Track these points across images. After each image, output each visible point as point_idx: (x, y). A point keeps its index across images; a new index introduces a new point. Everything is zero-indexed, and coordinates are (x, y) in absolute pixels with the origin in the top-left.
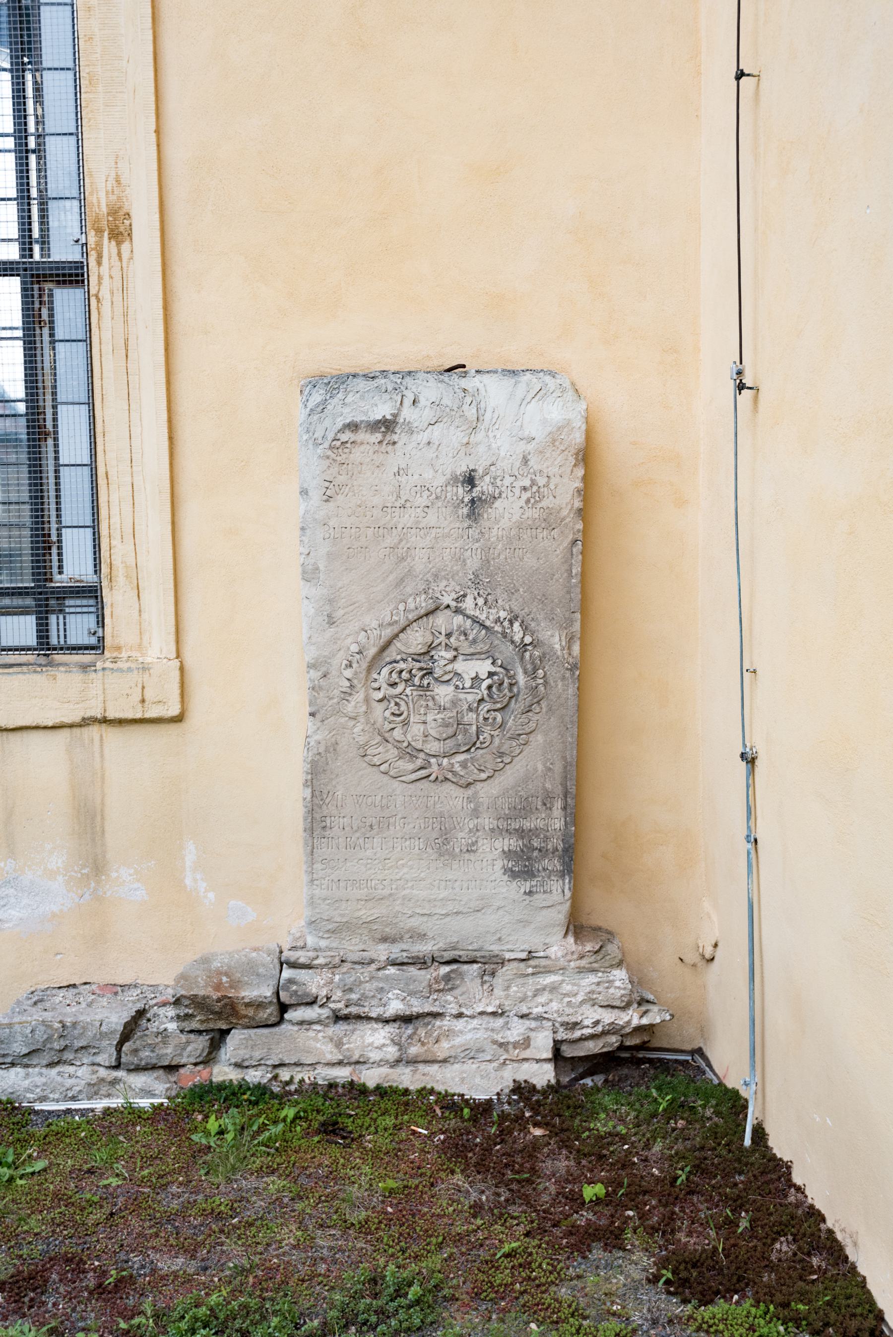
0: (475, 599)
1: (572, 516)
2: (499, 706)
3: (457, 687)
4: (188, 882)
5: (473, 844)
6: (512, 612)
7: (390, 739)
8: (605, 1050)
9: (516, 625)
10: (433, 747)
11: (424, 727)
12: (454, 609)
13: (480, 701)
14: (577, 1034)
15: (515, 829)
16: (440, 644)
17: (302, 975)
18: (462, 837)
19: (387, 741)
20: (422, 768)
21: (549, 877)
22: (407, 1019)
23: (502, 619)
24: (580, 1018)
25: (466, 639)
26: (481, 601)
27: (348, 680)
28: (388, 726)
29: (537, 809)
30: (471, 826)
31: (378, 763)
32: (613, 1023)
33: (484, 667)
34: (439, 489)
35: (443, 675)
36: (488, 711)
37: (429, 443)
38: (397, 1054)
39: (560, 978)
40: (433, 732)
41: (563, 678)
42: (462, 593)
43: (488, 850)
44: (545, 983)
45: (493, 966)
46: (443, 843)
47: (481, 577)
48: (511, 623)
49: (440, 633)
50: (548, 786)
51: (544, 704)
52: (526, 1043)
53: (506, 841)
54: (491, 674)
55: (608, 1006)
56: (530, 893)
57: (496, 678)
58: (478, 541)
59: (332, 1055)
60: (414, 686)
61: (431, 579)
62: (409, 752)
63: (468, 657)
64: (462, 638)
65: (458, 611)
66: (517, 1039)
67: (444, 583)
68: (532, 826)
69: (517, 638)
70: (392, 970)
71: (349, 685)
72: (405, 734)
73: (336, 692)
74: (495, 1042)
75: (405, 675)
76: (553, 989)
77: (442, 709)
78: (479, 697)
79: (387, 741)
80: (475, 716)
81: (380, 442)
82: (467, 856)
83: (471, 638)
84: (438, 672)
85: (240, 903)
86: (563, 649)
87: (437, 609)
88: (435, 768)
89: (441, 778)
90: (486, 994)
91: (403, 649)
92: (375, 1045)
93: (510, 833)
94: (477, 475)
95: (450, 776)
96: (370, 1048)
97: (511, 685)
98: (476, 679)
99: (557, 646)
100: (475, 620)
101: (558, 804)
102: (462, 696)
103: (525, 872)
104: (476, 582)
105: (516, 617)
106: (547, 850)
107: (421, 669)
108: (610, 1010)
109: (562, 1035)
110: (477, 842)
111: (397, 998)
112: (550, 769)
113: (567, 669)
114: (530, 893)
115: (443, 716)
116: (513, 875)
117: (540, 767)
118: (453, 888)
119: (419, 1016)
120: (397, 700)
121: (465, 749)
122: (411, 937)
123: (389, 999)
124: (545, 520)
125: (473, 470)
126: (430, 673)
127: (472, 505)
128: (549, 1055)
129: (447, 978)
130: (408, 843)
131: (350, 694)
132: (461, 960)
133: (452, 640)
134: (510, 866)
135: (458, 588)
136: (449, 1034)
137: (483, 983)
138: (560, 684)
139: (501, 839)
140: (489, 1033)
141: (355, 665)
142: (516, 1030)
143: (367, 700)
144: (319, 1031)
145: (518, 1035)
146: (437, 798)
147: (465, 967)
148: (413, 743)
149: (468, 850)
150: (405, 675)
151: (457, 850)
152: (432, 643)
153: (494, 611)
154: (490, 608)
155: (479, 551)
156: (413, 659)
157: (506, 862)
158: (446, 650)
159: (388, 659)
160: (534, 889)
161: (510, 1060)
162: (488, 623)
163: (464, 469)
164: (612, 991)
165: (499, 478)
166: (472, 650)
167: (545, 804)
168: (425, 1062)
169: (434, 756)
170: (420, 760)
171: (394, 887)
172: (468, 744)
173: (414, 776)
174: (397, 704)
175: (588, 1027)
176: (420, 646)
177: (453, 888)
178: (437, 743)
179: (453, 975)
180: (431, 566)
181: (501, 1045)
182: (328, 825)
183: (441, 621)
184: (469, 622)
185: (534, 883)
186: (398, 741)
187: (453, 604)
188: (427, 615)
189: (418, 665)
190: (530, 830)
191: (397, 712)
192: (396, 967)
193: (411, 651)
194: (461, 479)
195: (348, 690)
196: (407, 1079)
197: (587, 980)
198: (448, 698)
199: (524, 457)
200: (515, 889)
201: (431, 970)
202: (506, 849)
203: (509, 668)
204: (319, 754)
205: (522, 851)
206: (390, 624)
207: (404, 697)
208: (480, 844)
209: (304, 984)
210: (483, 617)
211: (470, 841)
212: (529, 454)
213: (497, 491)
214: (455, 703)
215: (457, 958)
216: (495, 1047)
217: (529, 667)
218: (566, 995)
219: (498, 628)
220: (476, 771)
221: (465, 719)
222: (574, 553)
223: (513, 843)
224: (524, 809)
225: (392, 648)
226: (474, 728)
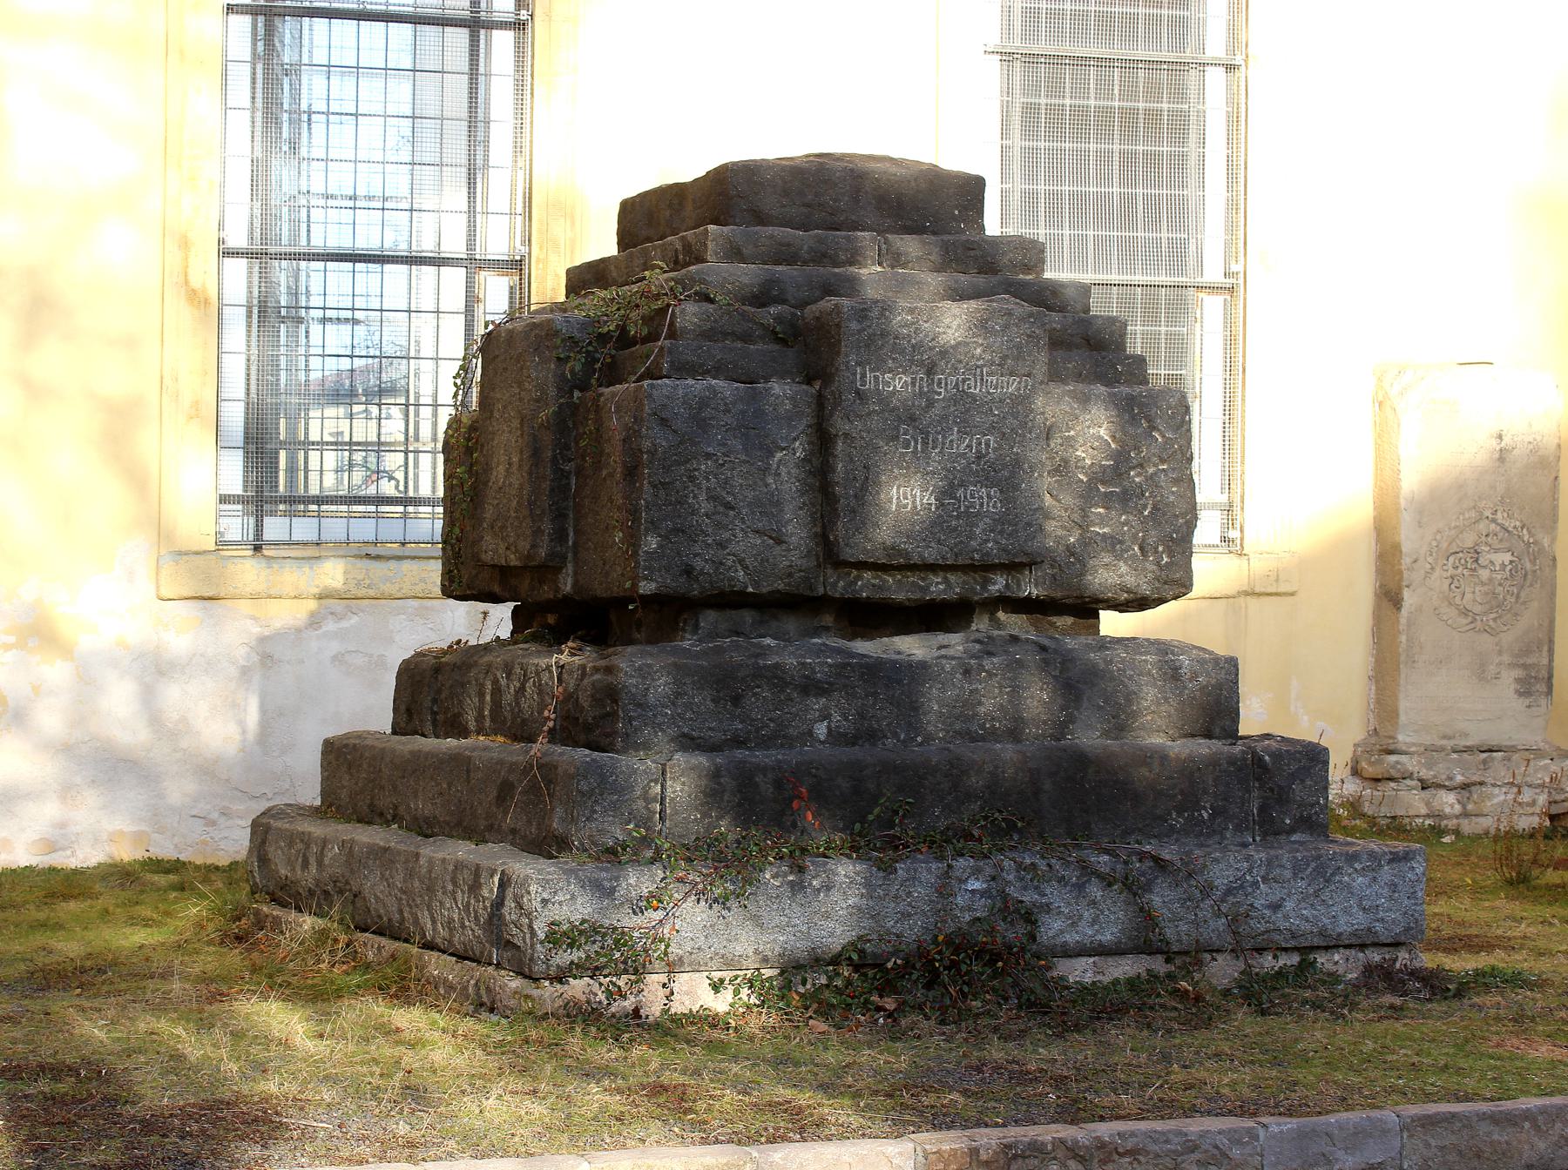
4: (1292, 708)
10: (1478, 609)
11: (1472, 596)
17: (1403, 758)
18: (1492, 668)
22: (1465, 786)
33: (1507, 557)
46: (1481, 673)
59: (1424, 811)
62: (1465, 612)
65: (1494, 521)
70: (1455, 756)
77: (1483, 584)
98: (1503, 565)
101: (1546, 648)
104: (1502, 502)
116: (1520, 694)
119: (1474, 784)
129: (1484, 762)
183: (1482, 526)
200: (1519, 704)
214: (1491, 580)
223: (1519, 673)
224: (1527, 652)
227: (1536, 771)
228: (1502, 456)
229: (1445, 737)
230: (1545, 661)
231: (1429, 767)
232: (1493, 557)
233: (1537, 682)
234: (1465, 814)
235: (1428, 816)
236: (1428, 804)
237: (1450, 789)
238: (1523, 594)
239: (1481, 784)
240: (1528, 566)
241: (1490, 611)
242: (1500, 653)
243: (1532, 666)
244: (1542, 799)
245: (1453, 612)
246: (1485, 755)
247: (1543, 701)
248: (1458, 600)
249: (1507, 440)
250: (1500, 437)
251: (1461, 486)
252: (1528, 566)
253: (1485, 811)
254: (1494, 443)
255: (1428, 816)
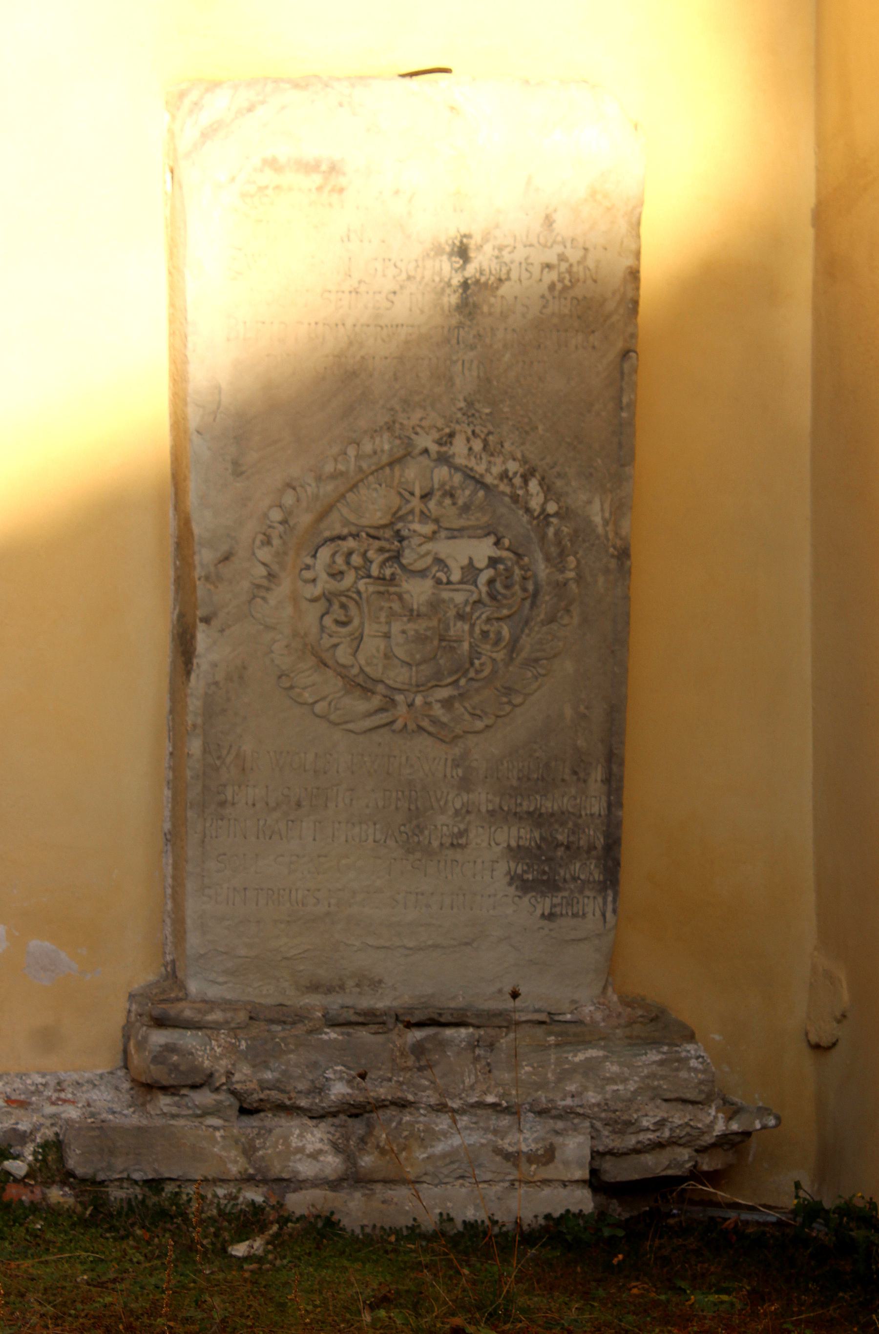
0: (468, 440)
1: (621, 311)
2: (505, 612)
3: (439, 582)
5: (461, 834)
6: (526, 462)
7: (330, 662)
8: (670, 1172)
9: (534, 485)
10: (399, 676)
11: (381, 644)
12: (434, 455)
13: (475, 602)
14: (631, 1141)
15: (529, 813)
16: (412, 512)
17: (189, 1040)
18: (444, 823)
19: (325, 665)
20: (382, 710)
21: (581, 892)
22: (356, 1110)
23: (510, 474)
24: (635, 1116)
25: (454, 504)
26: (477, 445)
27: (264, 564)
28: (327, 642)
29: (563, 780)
30: (458, 806)
31: (311, 700)
32: (687, 1124)
33: (482, 550)
34: (413, 264)
35: (415, 561)
36: (488, 620)
37: (397, 192)
38: (341, 1167)
39: (601, 1053)
40: (399, 652)
41: (607, 571)
42: (447, 430)
43: (485, 844)
44: (577, 1059)
45: (491, 1032)
46: (413, 831)
47: (477, 406)
48: (525, 480)
49: (412, 494)
50: (580, 743)
51: (576, 610)
52: (549, 1155)
53: (514, 831)
54: (493, 562)
55: (677, 1100)
56: (550, 917)
57: (501, 567)
58: (472, 347)
60: (369, 576)
61: (398, 407)
62: (361, 685)
63: (456, 533)
64: (448, 501)
65: (444, 459)
66: (533, 1146)
67: (419, 414)
68: (556, 807)
69: (535, 503)
70: (332, 1035)
71: (265, 573)
72: (355, 654)
73: (245, 585)
74: (498, 1151)
75: (356, 560)
76: (590, 1068)
77: (413, 615)
78: (475, 597)
79: (325, 665)
80: (467, 627)
81: (319, 189)
82: (450, 853)
83: (460, 502)
84: (408, 558)
85: (47, 944)
86: (606, 523)
87: (408, 454)
88: (402, 709)
89: (412, 726)
90: (481, 1077)
91: (352, 518)
92: (307, 1152)
93: (521, 818)
94: (472, 244)
95: (425, 724)
96: (298, 1156)
97: (525, 578)
98: (471, 571)
99: (598, 520)
100: (469, 475)
101: (598, 774)
102: (445, 595)
103: (543, 882)
104: (470, 411)
105: (532, 472)
106: (579, 848)
107: (381, 550)
108: (680, 1106)
109: (609, 1141)
110: (466, 830)
111: (341, 1079)
112: (584, 716)
113: (613, 556)
114: (550, 917)
115: (416, 627)
116: (524, 886)
117: (568, 712)
118: (428, 906)
119: (381, 1105)
120: (344, 599)
121: (450, 680)
122: (358, 985)
123: (327, 1079)
124: (579, 317)
125: (465, 236)
126: (396, 557)
127: (465, 291)
128: (582, 1173)
129: (419, 1049)
130: (357, 830)
131: (268, 589)
132: (442, 1020)
133: (432, 504)
134: (519, 871)
135: (440, 423)
136: (428, 1137)
137: (477, 1059)
138: (601, 580)
139: (506, 828)
140: (490, 1136)
141: (276, 542)
142: (527, 1137)
143: (295, 598)
144: (216, 1128)
145: (536, 1141)
146: (404, 759)
147: (449, 1032)
148: (367, 669)
149: (452, 845)
150: (356, 560)
151: (435, 844)
152: (399, 509)
153: (498, 460)
154: (492, 455)
155: (475, 363)
156: (368, 535)
157: (513, 865)
158: (420, 522)
159: (327, 534)
160: (558, 910)
161: (520, 1181)
162: (489, 480)
163: (452, 233)
164: (683, 1074)
165: (509, 249)
166: (462, 523)
167: (575, 773)
168: (385, 1181)
169: (400, 691)
170: (379, 697)
171: (333, 901)
172: (456, 672)
173: (368, 723)
174: (343, 606)
175: (648, 1129)
176: (379, 514)
177: (428, 906)
178: (405, 670)
179: (429, 1046)
180: (397, 386)
181: (507, 1156)
182: (230, 798)
183: (412, 474)
184: (458, 478)
185: (556, 901)
186: (344, 666)
187: (434, 448)
188: (391, 464)
189: (377, 544)
190: (552, 815)
191: (343, 618)
192: (338, 1029)
193: (364, 522)
194: (448, 249)
195: (265, 582)
196: (355, 1210)
197: (644, 1058)
198: (423, 598)
199: (547, 217)
200: (525, 911)
201: (393, 1036)
202: (513, 844)
203: (520, 551)
204: (216, 683)
205: (539, 847)
206: (333, 476)
207: (355, 596)
208: (472, 835)
209: (192, 1054)
210: (481, 468)
211: (456, 830)
212: (555, 211)
213: (504, 270)
214: (435, 605)
215: (436, 1016)
216: (498, 1159)
217: (554, 550)
218: (612, 1080)
219: (504, 487)
220: (467, 716)
221: (452, 632)
222: (626, 371)
225: (334, 516)
226: (466, 646)
227: (564, 1076)
228: (471, 298)
229: (315, 987)
230: (596, 806)
231: (259, 1057)
232: (443, 548)
233: (575, 852)
234: (353, 1179)
235: (248, 1180)
236: (249, 1151)
237: (318, 1116)
238: (526, 641)
239: (402, 1105)
240: (542, 570)
241: (436, 680)
242: (465, 784)
243: (560, 818)
244: (575, 1147)
245: (333, 684)
246: (419, 1034)
247: (591, 904)
248: (343, 655)
249: (482, 261)
250: (462, 252)
251: (354, 374)
252: (542, 570)
253: (411, 1172)
254: (446, 267)
255: (248, 1180)
